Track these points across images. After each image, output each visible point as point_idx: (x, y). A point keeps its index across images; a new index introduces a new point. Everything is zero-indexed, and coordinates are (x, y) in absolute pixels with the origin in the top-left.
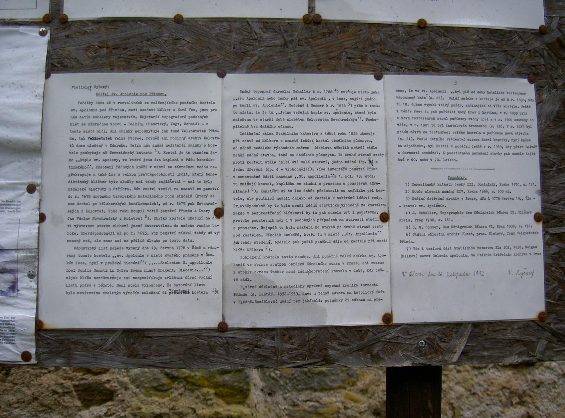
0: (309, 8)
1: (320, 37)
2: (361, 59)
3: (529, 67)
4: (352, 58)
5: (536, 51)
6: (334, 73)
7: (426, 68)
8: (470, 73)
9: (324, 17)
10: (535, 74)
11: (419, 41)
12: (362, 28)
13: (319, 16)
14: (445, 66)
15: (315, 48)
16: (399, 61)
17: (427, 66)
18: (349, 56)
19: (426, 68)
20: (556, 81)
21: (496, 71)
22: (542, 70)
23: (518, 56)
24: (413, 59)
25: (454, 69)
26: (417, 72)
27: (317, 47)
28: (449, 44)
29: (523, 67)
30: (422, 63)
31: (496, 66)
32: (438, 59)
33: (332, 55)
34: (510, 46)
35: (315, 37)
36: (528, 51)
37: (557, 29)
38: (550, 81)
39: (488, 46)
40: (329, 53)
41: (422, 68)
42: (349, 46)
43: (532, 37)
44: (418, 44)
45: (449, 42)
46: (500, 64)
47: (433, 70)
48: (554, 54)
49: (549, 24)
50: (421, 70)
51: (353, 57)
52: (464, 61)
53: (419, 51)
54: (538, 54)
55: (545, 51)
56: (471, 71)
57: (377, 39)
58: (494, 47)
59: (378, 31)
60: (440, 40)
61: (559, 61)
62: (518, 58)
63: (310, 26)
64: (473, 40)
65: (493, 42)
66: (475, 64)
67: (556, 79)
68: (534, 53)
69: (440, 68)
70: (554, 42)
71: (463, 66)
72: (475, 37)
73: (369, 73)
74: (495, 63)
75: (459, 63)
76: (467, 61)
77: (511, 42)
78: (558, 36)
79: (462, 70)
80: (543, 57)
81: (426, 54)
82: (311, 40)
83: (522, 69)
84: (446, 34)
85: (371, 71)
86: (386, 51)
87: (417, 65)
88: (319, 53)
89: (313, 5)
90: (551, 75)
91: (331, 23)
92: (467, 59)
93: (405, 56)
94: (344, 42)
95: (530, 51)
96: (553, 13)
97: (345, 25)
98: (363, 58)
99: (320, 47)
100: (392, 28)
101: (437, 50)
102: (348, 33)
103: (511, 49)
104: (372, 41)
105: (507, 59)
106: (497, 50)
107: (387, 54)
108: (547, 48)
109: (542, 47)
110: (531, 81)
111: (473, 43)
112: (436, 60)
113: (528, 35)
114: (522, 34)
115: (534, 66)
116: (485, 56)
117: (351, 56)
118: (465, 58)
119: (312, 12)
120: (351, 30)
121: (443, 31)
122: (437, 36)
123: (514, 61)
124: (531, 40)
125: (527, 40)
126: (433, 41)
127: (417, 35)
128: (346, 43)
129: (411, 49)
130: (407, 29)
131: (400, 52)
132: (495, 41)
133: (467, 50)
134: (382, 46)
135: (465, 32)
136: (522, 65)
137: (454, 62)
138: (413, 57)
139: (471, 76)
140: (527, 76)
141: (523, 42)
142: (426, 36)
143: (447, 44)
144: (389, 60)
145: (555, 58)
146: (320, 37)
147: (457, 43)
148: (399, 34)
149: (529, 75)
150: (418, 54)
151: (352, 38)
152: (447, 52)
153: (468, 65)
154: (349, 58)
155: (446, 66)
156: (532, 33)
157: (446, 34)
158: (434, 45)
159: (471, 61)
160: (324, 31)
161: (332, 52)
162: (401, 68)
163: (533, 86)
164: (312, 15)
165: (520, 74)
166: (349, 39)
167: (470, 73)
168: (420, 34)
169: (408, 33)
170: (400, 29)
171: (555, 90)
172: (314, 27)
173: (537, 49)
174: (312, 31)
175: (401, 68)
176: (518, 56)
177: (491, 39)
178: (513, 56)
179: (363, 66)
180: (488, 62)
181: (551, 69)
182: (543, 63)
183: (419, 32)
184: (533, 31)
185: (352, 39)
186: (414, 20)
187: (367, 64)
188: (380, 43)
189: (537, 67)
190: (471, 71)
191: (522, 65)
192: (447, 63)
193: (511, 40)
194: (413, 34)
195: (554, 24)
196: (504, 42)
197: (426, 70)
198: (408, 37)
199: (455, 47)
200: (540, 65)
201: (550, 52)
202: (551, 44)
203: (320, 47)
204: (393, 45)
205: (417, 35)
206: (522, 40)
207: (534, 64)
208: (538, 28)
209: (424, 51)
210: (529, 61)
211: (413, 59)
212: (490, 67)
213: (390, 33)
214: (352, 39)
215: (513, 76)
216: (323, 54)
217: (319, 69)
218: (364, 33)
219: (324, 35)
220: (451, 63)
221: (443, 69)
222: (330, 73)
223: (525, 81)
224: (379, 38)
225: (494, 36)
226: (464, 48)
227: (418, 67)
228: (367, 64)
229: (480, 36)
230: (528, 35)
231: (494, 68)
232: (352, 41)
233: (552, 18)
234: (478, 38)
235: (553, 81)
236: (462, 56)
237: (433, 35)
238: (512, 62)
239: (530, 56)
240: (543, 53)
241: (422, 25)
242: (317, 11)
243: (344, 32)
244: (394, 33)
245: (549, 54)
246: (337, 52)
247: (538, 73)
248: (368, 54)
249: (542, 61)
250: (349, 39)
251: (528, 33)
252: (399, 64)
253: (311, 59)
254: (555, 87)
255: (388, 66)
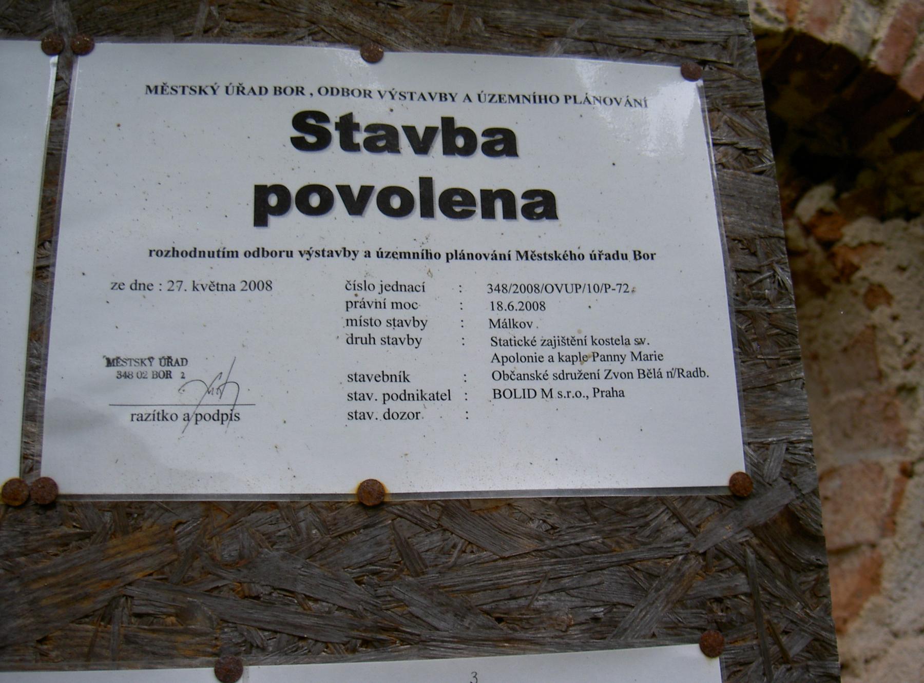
0: (24, 457)
1: (52, 550)
2: (177, 616)
3: (703, 605)
4: (149, 615)
5: (720, 554)
6: (86, 668)
7: (383, 637)
8: (521, 640)
9: (65, 488)
10: (721, 627)
11: (363, 549)
12: (184, 516)
13: (49, 484)
14: (442, 625)
15: (34, 586)
16: (298, 620)
17: (385, 630)
18: (137, 610)
19: (383, 637)
20: (784, 639)
21: (604, 630)
22: (743, 610)
23: (670, 575)
24: (341, 608)
25: (471, 633)
26: (354, 650)
27: (42, 584)
28: (455, 553)
29: (684, 607)
30: (369, 619)
31: (600, 611)
32: (419, 604)
33: (86, 606)
34: (644, 544)
35: (36, 550)
36: (698, 554)
37: (781, 480)
38: (769, 640)
39: (577, 549)
40: (76, 600)
41: (368, 635)
42: (139, 576)
43: (708, 511)
44: (356, 559)
45: (454, 546)
46: (614, 605)
47: (403, 641)
48: (776, 555)
49: (756, 465)
50: (366, 643)
51: (150, 610)
52: (503, 606)
53: (359, 583)
54: (729, 563)
55: (749, 550)
56: (529, 635)
57: (228, 551)
58: (594, 551)
59: (234, 523)
60: (427, 543)
61: (793, 575)
62: (670, 580)
63: (21, 515)
64: (529, 536)
65: (593, 539)
66: (538, 611)
67: (786, 632)
68: (716, 559)
69: (425, 633)
70: (774, 522)
71: (499, 620)
72: (533, 525)
73: (197, 661)
74: (598, 603)
75: (487, 613)
76: (513, 604)
77: (647, 532)
78: (786, 501)
79: (493, 634)
80: (743, 569)
81: (381, 591)
82: (22, 559)
83: (683, 614)
84: (446, 522)
85: (205, 654)
86: (257, 589)
87: (352, 627)
88: (44, 602)
89: (37, 447)
90: (769, 622)
91: (86, 506)
92: (513, 598)
93: (316, 600)
94: (125, 563)
95: (704, 554)
96: (769, 434)
97: (128, 512)
98: (183, 615)
99: (52, 580)
100: (275, 513)
101: (417, 575)
102: (138, 534)
103: (646, 555)
104: (213, 558)
105: (635, 588)
106: (602, 560)
107: (257, 598)
108: (755, 541)
109: (740, 538)
110: (709, 651)
111: (528, 545)
112: (413, 609)
113: (696, 506)
114: (677, 505)
115: (719, 600)
116: (566, 582)
117: (144, 609)
118: (504, 593)
119: (31, 469)
120: (145, 525)
121: (436, 515)
122: (418, 529)
123: (657, 590)
124: (707, 519)
125: (693, 522)
126: (404, 546)
127: (357, 530)
128: (129, 568)
129: (337, 579)
130: (324, 512)
131: (300, 588)
132: (597, 532)
133: (511, 568)
134: (245, 571)
135: (504, 511)
136: (681, 602)
137: (469, 609)
138: (343, 604)
139: (524, 651)
140: (698, 634)
141: (682, 529)
142: (382, 533)
143: (449, 554)
144: (266, 615)
145: (780, 570)
146: (52, 550)
147: (481, 549)
148: (298, 533)
149: (702, 629)
150: (357, 591)
151: (152, 549)
152: (447, 581)
153: (515, 615)
154: (139, 616)
155: (446, 624)
156: (708, 498)
157: (446, 522)
158: (408, 560)
159: (522, 602)
160: (65, 529)
161: (87, 596)
162: (302, 638)
163: (716, 663)
164: (30, 481)
165: (675, 633)
166: (140, 552)
167: (521, 640)
168: (366, 527)
169: (326, 527)
170: (301, 514)
171: (783, 668)
172: (33, 519)
173: (726, 548)
174: (26, 533)
175: (302, 638)
176: (670, 575)
177: (584, 530)
178: (651, 576)
179: (180, 638)
180: (577, 602)
181: (769, 606)
182: (745, 588)
183: (361, 520)
184: (712, 494)
185: (152, 555)
186: (345, 484)
187: (196, 634)
188: (243, 561)
189: (728, 603)
190: (529, 635)
191: (681, 602)
192: (449, 616)
193: (647, 524)
194: (344, 529)
195: (773, 468)
196: (625, 535)
197: (380, 641)
198: (327, 538)
199: (472, 563)
200: (736, 596)
201: (763, 552)
202: (766, 525)
203: (52, 580)
204: (279, 569)
205: (357, 530)
206: (680, 521)
207: (717, 594)
208: (725, 482)
209: (375, 579)
210: (701, 587)
211: (341, 608)
212: (582, 618)
213: (272, 528)
214: (152, 555)
215: (653, 639)
216: (57, 606)
217: (44, 654)
218: (189, 534)
219: (64, 542)
220: (460, 614)
221: (436, 635)
222: (73, 668)
223: (693, 650)
224: (237, 546)
225: (595, 519)
226: (501, 563)
227: (355, 633)
228: (196, 634)
229: (551, 521)
230: (696, 506)
231: (596, 619)
232: (149, 562)
233: (765, 446)
234: (545, 527)
235: (777, 642)
236: (497, 587)
237: (405, 529)
238: (652, 594)
239: (706, 568)
240: (745, 556)
241: (371, 498)
242: (46, 471)
243: (125, 533)
244: (284, 528)
245: (760, 558)
246: (101, 598)
247: (730, 622)
248: (198, 601)
249: (741, 582)
250: (140, 552)
251: (696, 499)
252: (296, 626)
253: (20, 622)
254: (784, 658)
255: (260, 637)
